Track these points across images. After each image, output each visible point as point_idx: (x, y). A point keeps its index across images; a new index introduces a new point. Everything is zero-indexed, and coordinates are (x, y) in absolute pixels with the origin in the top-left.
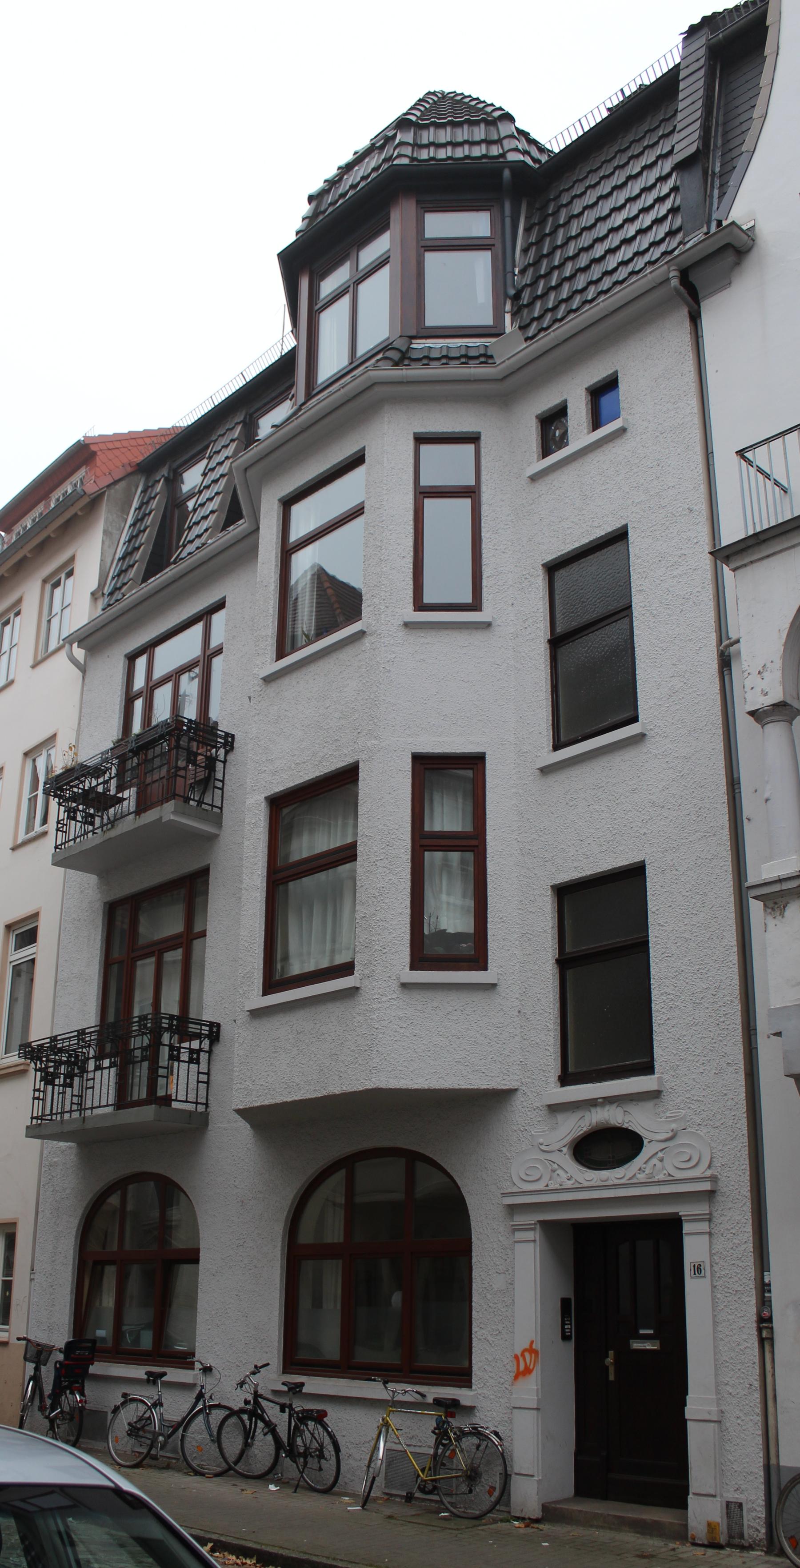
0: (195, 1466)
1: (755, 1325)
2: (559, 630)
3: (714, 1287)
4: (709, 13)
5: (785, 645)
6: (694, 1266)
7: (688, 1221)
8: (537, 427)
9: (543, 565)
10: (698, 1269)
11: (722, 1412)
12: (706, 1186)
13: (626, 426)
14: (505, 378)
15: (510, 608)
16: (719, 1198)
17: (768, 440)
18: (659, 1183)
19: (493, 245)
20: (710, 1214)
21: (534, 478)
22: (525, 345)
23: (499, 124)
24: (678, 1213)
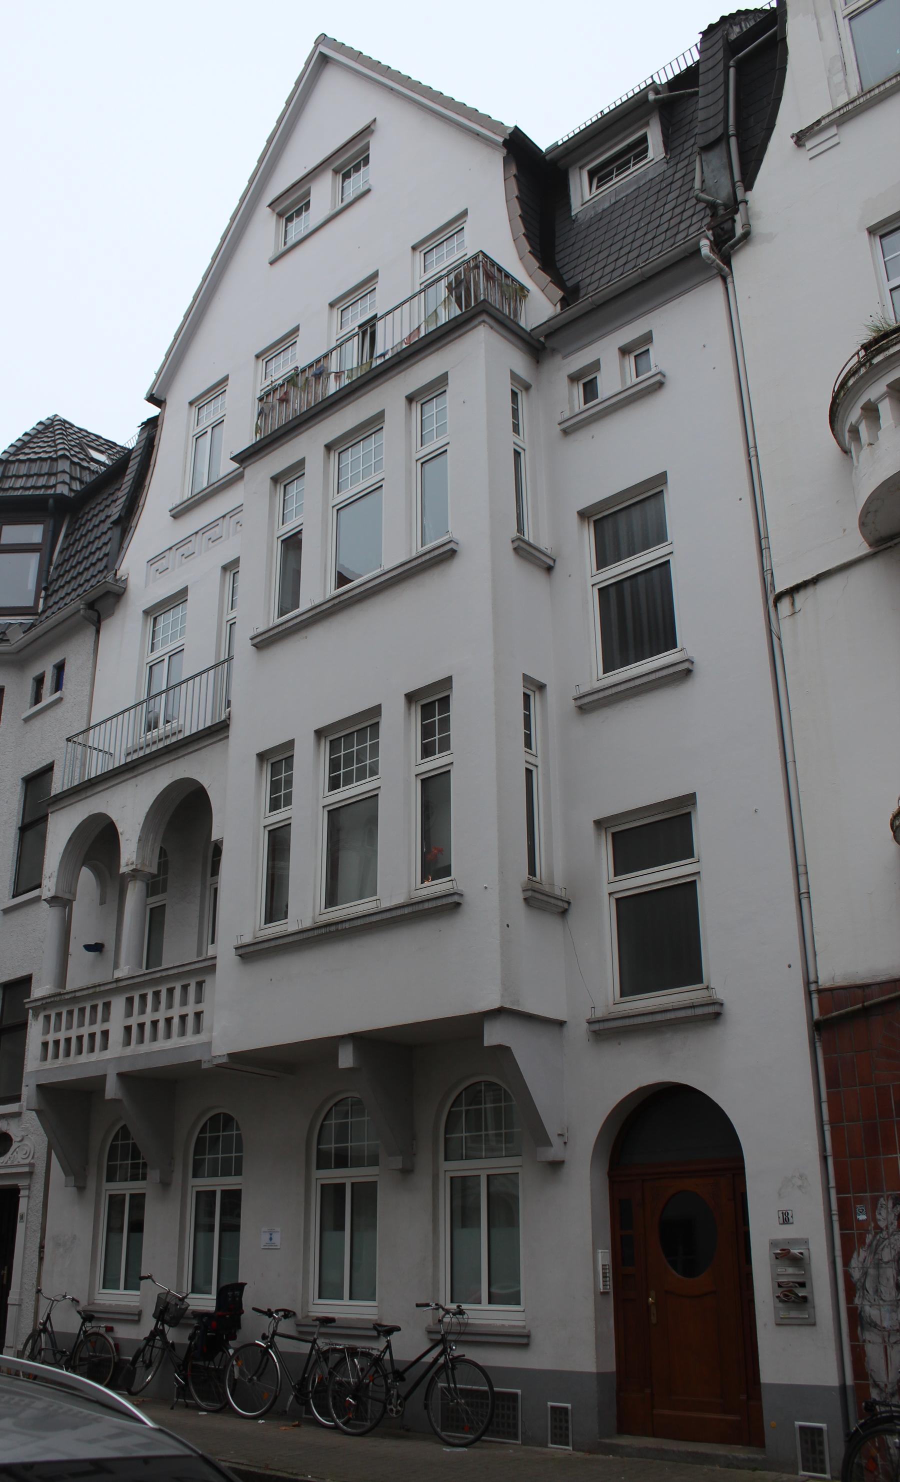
0: (489, 1410)
1: (38, 1250)
2: (26, 821)
3: (26, 1228)
4: (727, 14)
5: (61, 862)
6: (783, 1213)
7: (23, 1189)
8: (33, 685)
9: (22, 779)
10: (22, 1217)
11: (22, 1300)
12: (26, 1169)
13: (62, 697)
14: (20, 651)
15: (5, 804)
16: (34, 1176)
17: (110, 719)
18: (17, 1166)
19: (41, 549)
20: (29, 1185)
21: (27, 720)
22: (23, 635)
23: (59, 461)
24: (17, 1184)
